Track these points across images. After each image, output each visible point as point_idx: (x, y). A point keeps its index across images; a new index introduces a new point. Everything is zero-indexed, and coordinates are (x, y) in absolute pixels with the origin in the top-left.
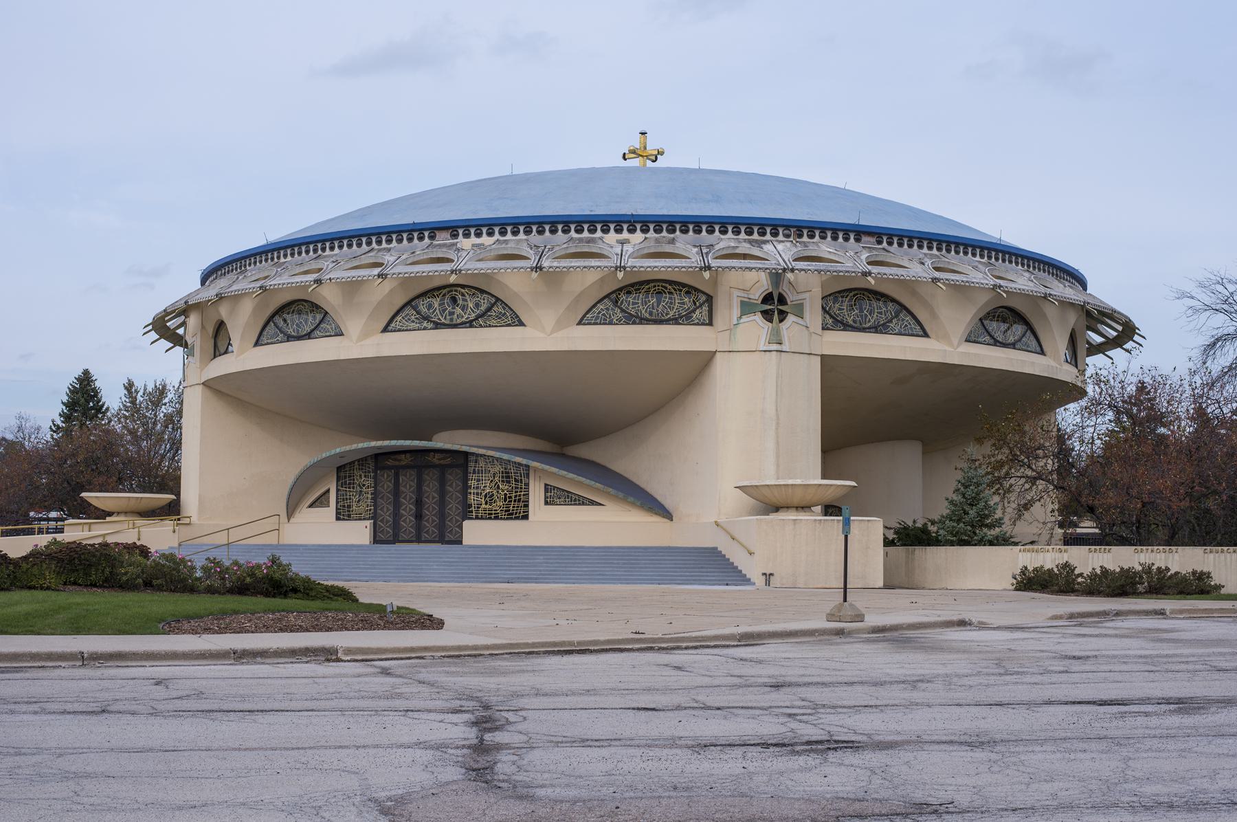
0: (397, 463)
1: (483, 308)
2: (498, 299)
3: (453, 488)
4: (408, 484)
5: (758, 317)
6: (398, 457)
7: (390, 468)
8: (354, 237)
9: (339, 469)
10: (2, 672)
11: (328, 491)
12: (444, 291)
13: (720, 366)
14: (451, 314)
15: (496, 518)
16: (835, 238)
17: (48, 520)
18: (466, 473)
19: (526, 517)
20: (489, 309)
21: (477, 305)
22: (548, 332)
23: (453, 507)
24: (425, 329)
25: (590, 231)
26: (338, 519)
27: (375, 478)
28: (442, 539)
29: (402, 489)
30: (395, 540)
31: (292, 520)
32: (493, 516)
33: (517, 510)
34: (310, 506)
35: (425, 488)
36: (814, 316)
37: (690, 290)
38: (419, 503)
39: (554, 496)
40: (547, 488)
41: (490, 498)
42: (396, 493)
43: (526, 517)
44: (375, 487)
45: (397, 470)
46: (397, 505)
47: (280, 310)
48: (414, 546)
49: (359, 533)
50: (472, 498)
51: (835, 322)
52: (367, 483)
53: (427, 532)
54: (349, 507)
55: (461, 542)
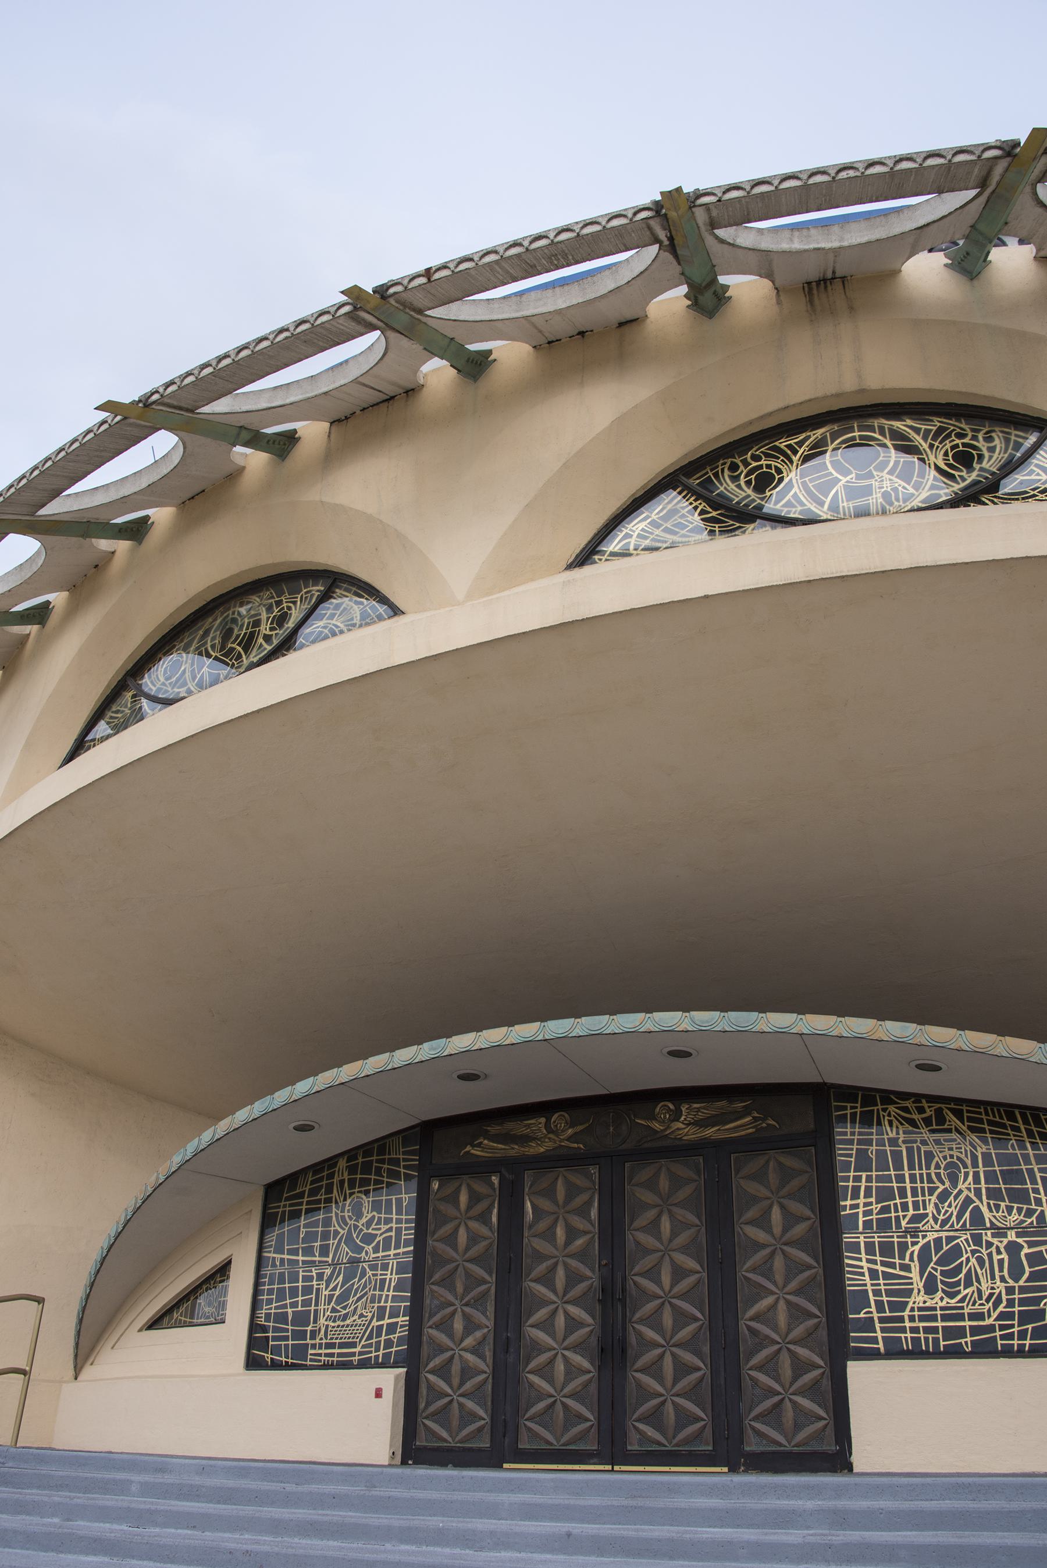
0: (515, 1150)
3: (770, 1227)
4: (561, 1228)
6: (518, 1127)
7: (481, 1169)
9: (273, 1191)
10: (6, 1484)
11: (223, 1271)
15: (985, 1350)
23: (774, 1307)
26: (253, 1363)
28: (728, 1446)
29: (533, 1243)
30: (502, 1444)
31: (84, 1375)
34: (154, 1324)
35: (637, 1236)
38: (613, 1298)
41: (946, 1265)
42: (509, 1260)
45: (513, 1175)
46: (511, 1308)
50: (861, 1269)
52: (380, 1232)
53: (654, 1418)
54: (302, 1318)
55: (836, 1457)
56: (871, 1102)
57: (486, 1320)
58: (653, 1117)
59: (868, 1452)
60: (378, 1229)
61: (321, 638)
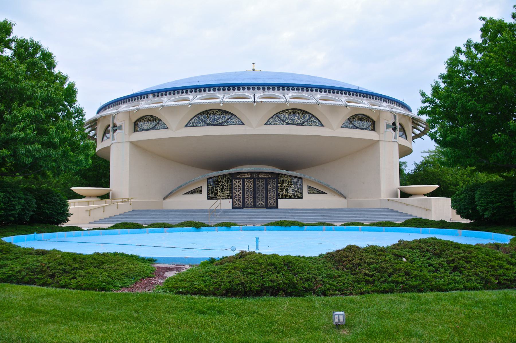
1: (307, 119)
2: (313, 115)
5: (391, 129)
7: (240, 179)
8: (172, 90)
12: (291, 111)
13: (382, 146)
14: (294, 120)
15: (290, 198)
17: (331, 284)
18: (277, 181)
19: (301, 198)
21: (304, 117)
22: (334, 130)
24: (283, 125)
30: (243, 207)
33: (299, 196)
36: (127, 126)
37: (368, 118)
39: (311, 190)
40: (309, 187)
43: (301, 198)
47: (203, 113)
49: (226, 204)
51: (136, 127)
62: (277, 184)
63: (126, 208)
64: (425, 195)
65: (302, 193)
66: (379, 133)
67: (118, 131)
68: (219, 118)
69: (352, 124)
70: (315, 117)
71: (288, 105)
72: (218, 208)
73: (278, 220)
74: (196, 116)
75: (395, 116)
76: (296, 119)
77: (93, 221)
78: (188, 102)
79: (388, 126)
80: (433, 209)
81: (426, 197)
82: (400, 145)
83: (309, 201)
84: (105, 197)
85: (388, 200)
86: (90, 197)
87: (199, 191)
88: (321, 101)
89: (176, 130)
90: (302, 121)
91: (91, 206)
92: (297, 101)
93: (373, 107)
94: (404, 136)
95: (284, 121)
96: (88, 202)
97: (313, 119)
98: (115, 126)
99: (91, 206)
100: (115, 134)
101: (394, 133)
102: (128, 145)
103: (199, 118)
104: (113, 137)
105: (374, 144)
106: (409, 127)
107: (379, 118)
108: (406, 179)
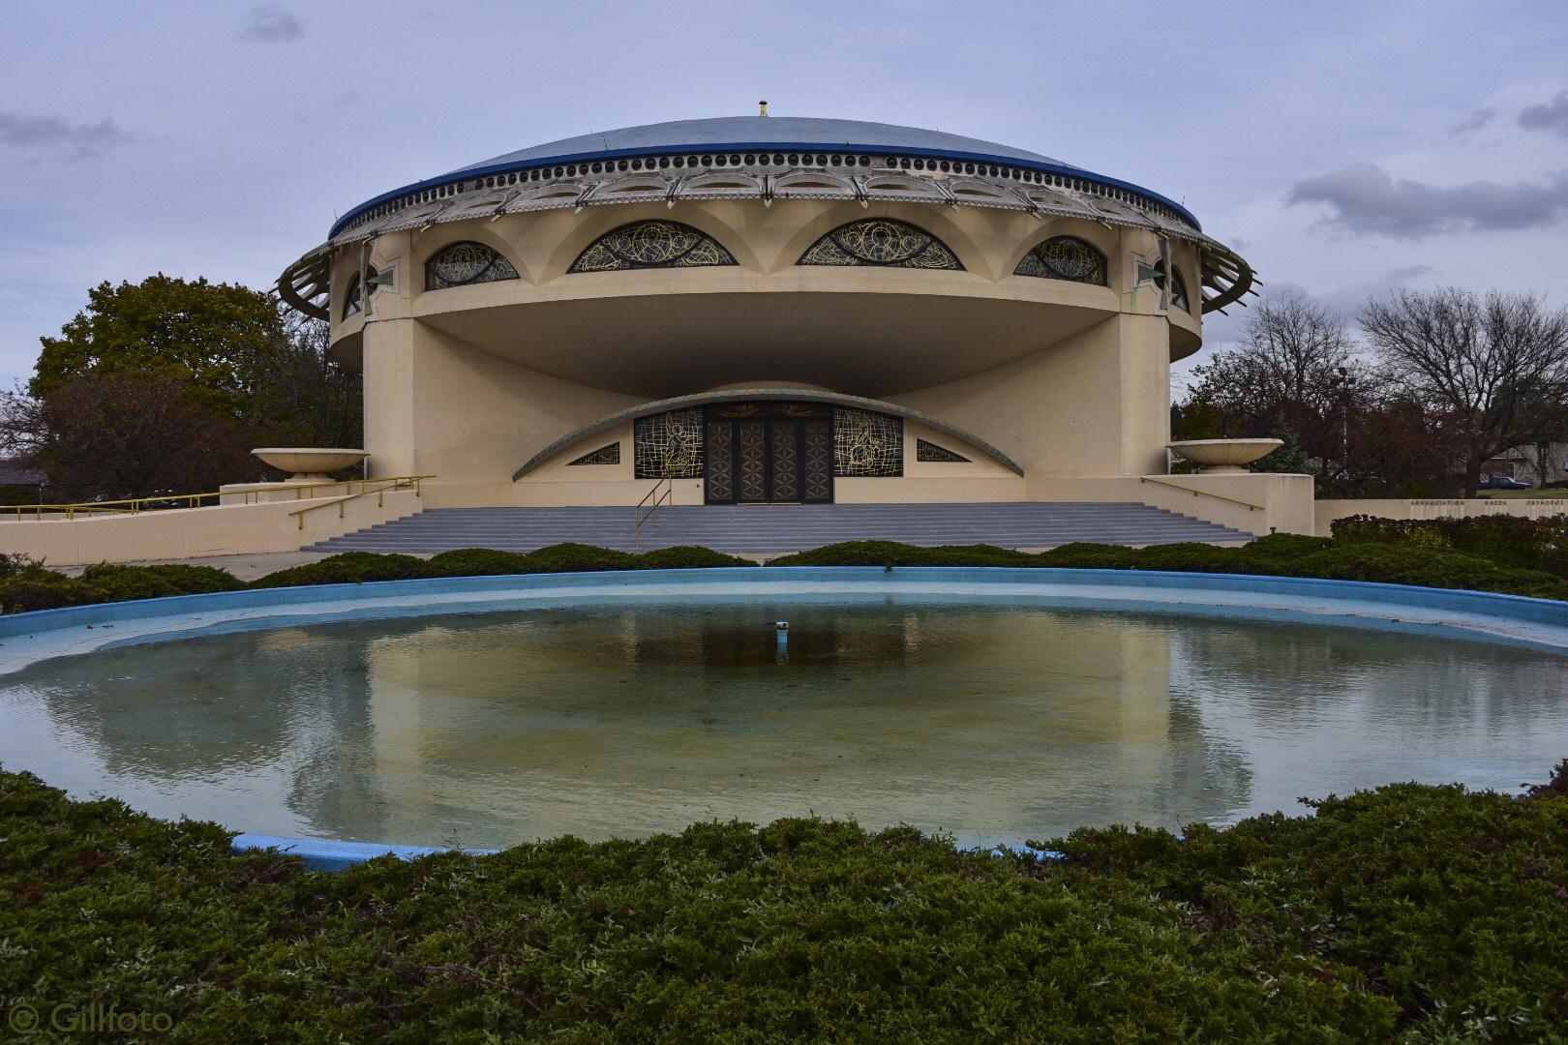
2: (934, 238)
4: (752, 439)
5: (1152, 283)
8: (756, 151)
14: (879, 250)
15: (867, 475)
16: (610, 169)
19: (900, 474)
20: (923, 249)
21: (910, 244)
22: (990, 279)
23: (814, 463)
25: (819, 162)
27: (705, 431)
28: (802, 498)
30: (735, 499)
32: (858, 473)
33: (893, 468)
36: (405, 273)
37: (1090, 249)
39: (927, 453)
40: (920, 444)
42: (736, 446)
43: (900, 474)
44: (705, 440)
47: (617, 232)
48: (797, 507)
49: (688, 492)
51: (431, 278)
55: (831, 500)
56: (839, 406)
57: (729, 465)
58: (1247, 876)
59: (838, 500)
60: (690, 438)
61: (1235, 533)
62: (832, 434)
63: (403, 506)
64: (1243, 466)
65: (900, 462)
66: (1120, 294)
67: (380, 288)
68: (665, 247)
69: (1046, 265)
70: (940, 242)
71: (865, 204)
72: (665, 502)
73: (666, 544)
74: (598, 240)
75: (1162, 243)
76: (887, 247)
77: (310, 543)
78: (574, 199)
79: (1144, 272)
80: (1269, 507)
81: (1246, 473)
82: (1173, 328)
83: (924, 483)
84: (354, 472)
85: (1143, 480)
86: (306, 474)
87: (610, 455)
88: (960, 197)
89: (541, 283)
90: (905, 255)
91: (306, 502)
92: (882, 190)
93: (1107, 215)
94: (1180, 301)
95: (852, 255)
96: (299, 488)
97: (934, 249)
98: (371, 272)
99: (306, 502)
100: (372, 297)
101: (1159, 291)
102: (408, 329)
103: (607, 248)
104: (368, 304)
105: (1108, 317)
106: (1192, 272)
107: (1118, 247)
108: (1188, 421)
